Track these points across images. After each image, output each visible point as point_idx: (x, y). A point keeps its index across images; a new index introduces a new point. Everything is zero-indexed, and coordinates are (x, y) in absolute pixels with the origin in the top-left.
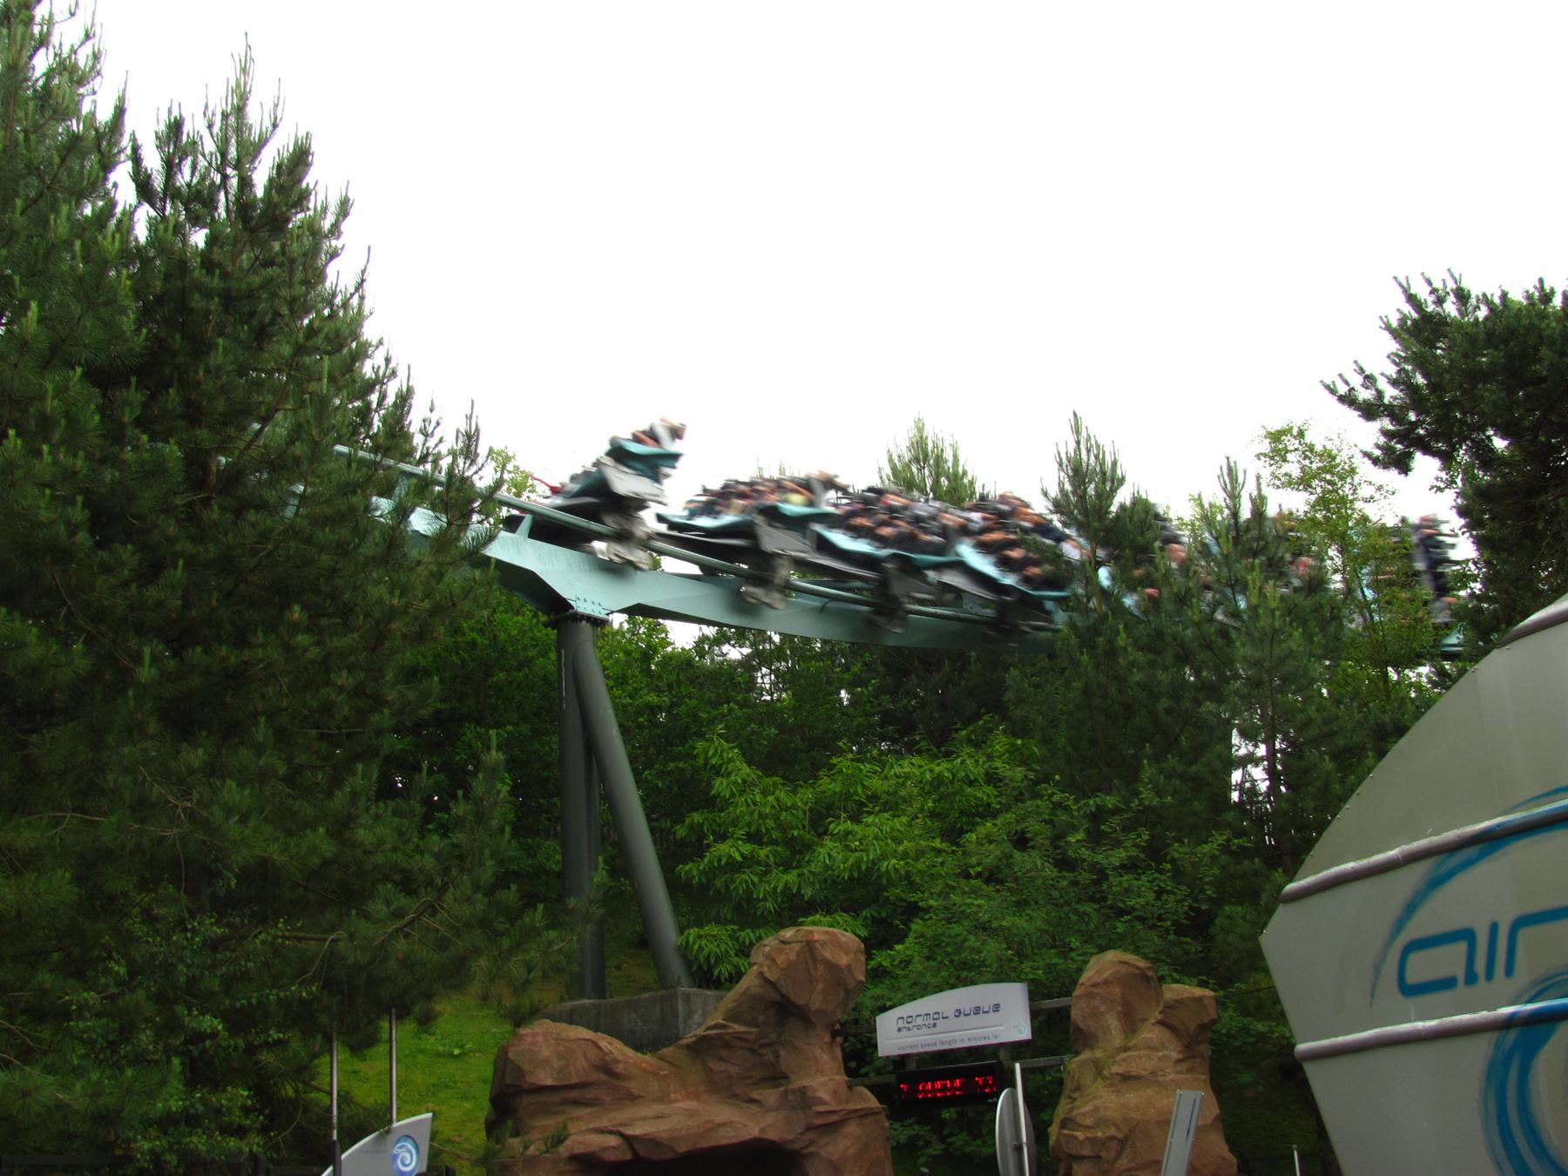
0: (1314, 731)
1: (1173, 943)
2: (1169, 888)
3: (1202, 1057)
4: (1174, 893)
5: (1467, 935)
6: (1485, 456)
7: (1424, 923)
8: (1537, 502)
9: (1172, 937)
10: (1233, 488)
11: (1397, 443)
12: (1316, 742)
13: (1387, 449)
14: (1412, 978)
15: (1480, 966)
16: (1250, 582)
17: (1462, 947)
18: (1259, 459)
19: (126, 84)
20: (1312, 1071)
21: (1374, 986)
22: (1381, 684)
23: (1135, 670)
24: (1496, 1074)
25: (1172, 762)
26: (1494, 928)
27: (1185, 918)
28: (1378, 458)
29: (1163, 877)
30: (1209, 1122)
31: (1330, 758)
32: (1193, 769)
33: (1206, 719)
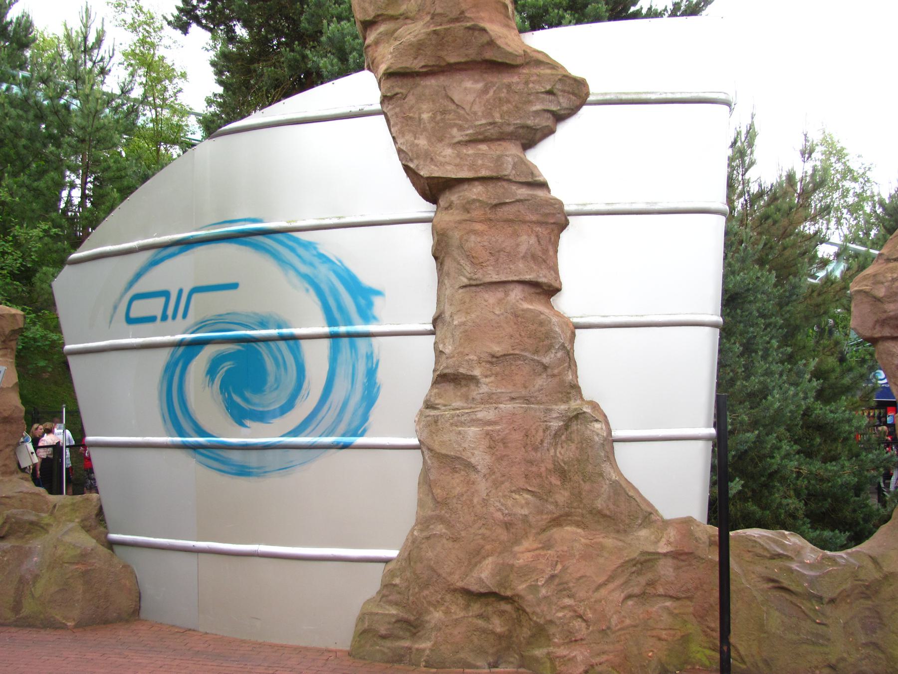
0: (110, 174)
1: (7, 284)
2: (10, 251)
3: (12, 349)
4: (12, 255)
5: (166, 294)
6: (231, 37)
7: (146, 284)
8: (252, 67)
9: (8, 280)
10: (87, 21)
11: (184, 16)
12: (112, 180)
13: (178, 19)
14: (133, 314)
15: (170, 312)
16: (87, 79)
17: (161, 301)
20: (71, 360)
21: (112, 317)
22: (155, 154)
23: (7, 118)
24: (169, 369)
25: (23, 178)
26: (181, 292)
27: (18, 270)
28: (171, 21)
29: (7, 245)
30: (10, 386)
31: (117, 191)
32: (36, 184)
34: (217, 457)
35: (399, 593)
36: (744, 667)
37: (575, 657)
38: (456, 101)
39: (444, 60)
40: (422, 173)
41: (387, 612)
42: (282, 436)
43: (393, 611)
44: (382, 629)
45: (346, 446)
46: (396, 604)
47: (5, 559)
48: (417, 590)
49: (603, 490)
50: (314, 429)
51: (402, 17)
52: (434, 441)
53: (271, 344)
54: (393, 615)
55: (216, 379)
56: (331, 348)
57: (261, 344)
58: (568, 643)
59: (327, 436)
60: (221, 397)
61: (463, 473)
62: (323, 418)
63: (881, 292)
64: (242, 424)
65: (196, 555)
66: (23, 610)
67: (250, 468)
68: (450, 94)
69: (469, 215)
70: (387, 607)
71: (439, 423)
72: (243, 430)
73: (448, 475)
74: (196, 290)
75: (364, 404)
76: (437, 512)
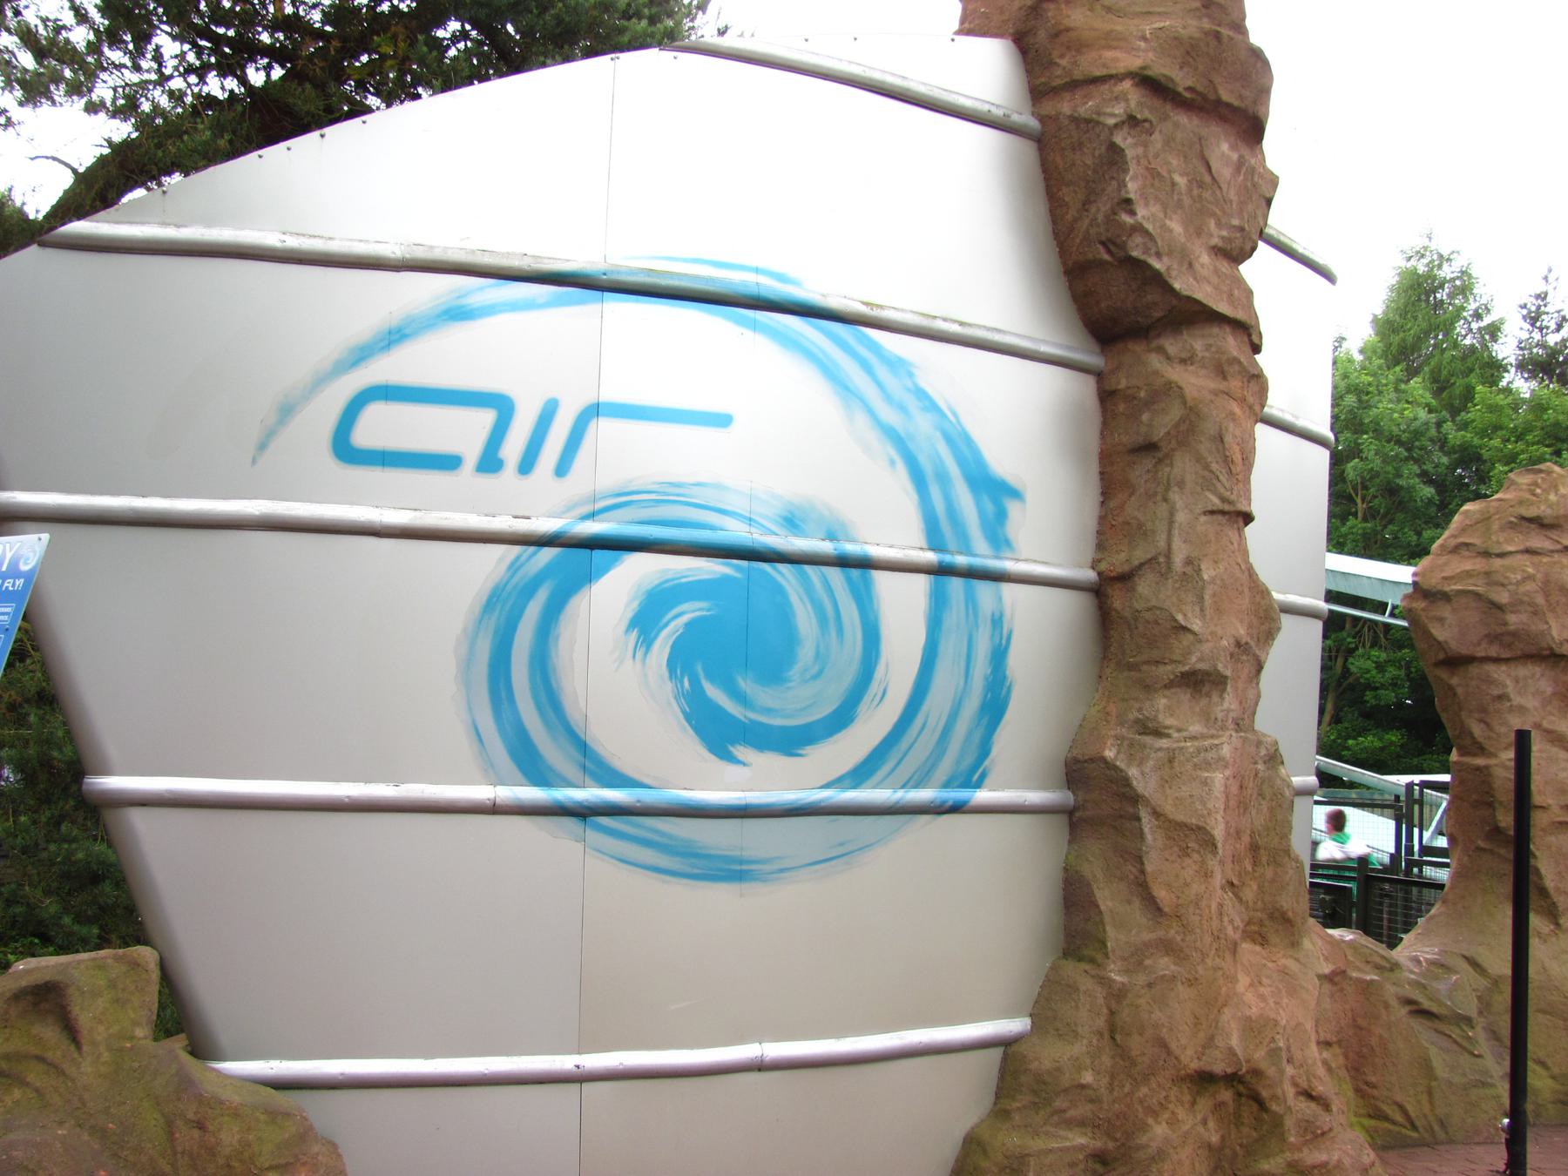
5: (502, 406)
15: (512, 448)
17: (484, 419)
18: (1538, 297)
19: (47, 158)
33: (1216, 1132)
34: (650, 836)
35: (1091, 1101)
36: (1415, 1135)
37: (1339, 1161)
38: (1213, 171)
39: (1216, 91)
40: (1177, 286)
42: (827, 786)
45: (956, 808)
46: (1081, 1123)
49: (1288, 877)
50: (893, 770)
52: (1166, 797)
53: (808, 569)
54: (1082, 1148)
55: (657, 644)
58: (1311, 1141)
59: (916, 786)
60: (669, 686)
61: (1196, 856)
63: (1503, 597)
65: (575, 1087)
67: (741, 862)
68: (1207, 154)
69: (1225, 383)
70: (1062, 1133)
71: (1176, 764)
72: (731, 770)
74: (594, 411)
75: (985, 721)
76: (1161, 933)
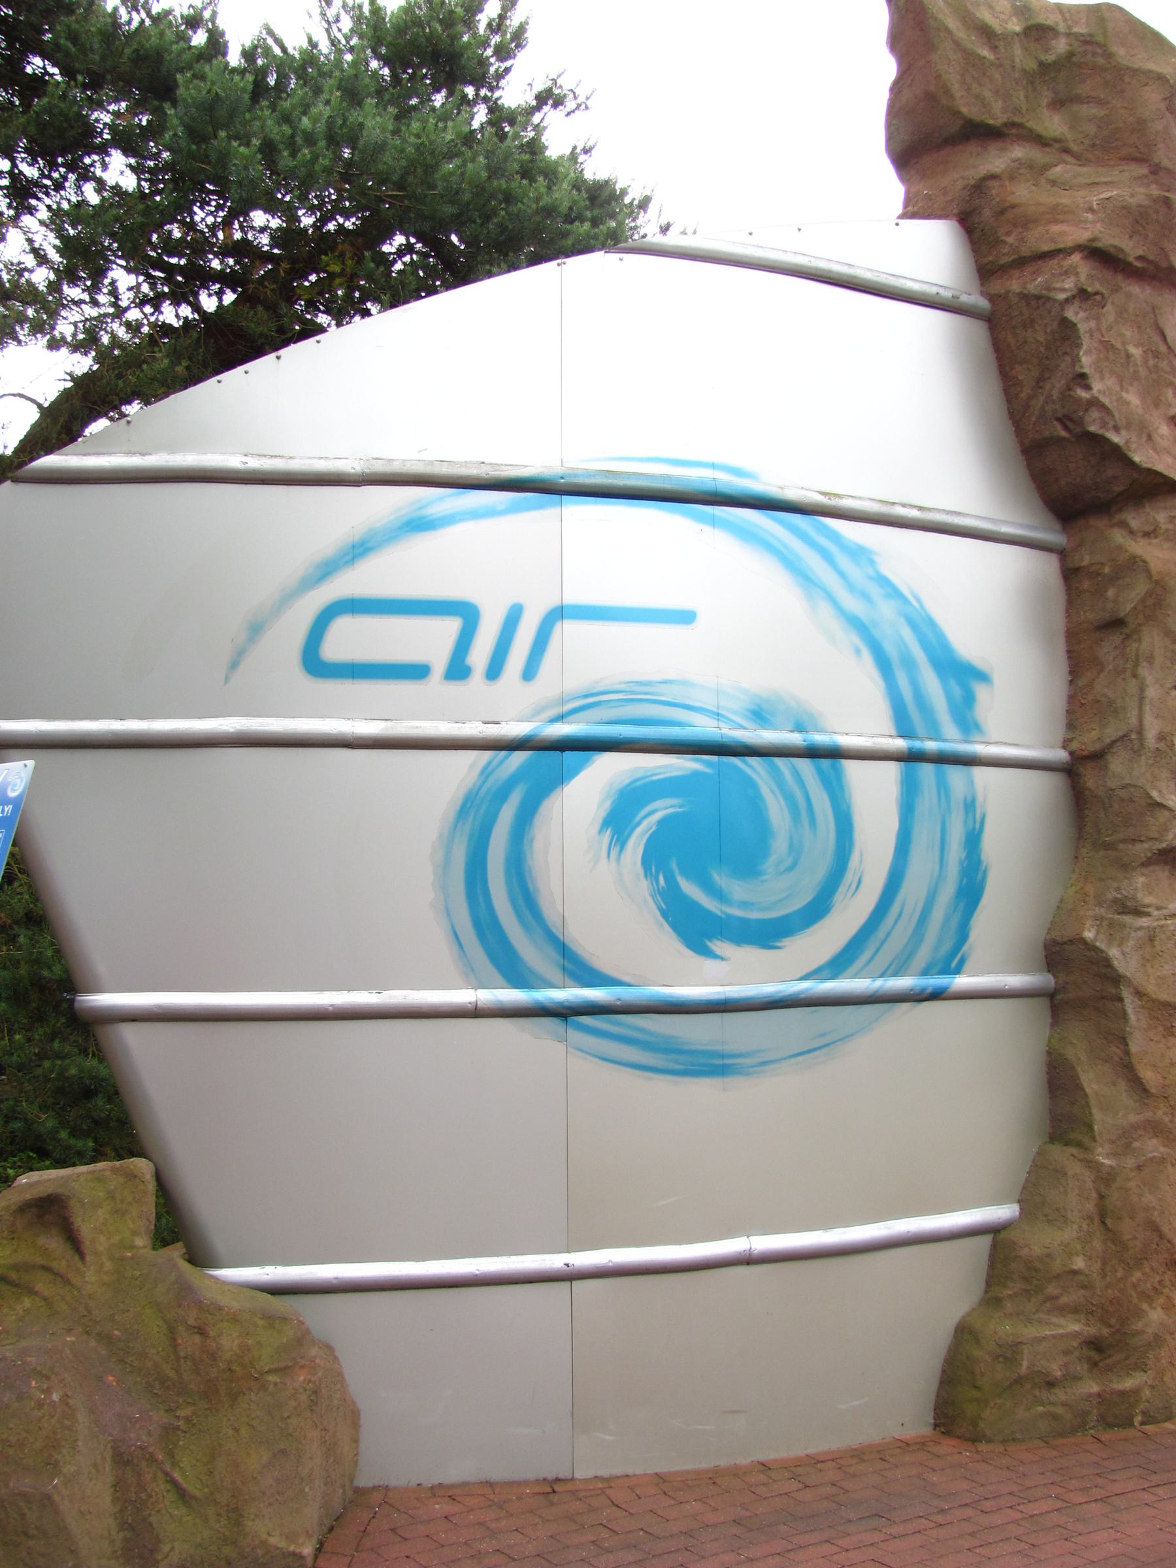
5: (467, 613)
15: (479, 655)
17: (451, 627)
39: (1167, 257)
40: (1137, 459)
41: (1061, 1331)
43: (1073, 1326)
44: (1055, 1367)
45: (936, 995)
46: (1074, 1310)
47: (55, 1397)
48: (1119, 1274)
51: (1057, 146)
54: (1076, 1335)
56: (902, 783)
57: (753, 761)
59: (895, 974)
62: (888, 934)
64: (707, 953)
66: (166, 1548)
67: (723, 1056)
70: (1055, 1320)
72: (709, 965)
73: (1158, 1042)
74: (558, 614)
75: (961, 906)
